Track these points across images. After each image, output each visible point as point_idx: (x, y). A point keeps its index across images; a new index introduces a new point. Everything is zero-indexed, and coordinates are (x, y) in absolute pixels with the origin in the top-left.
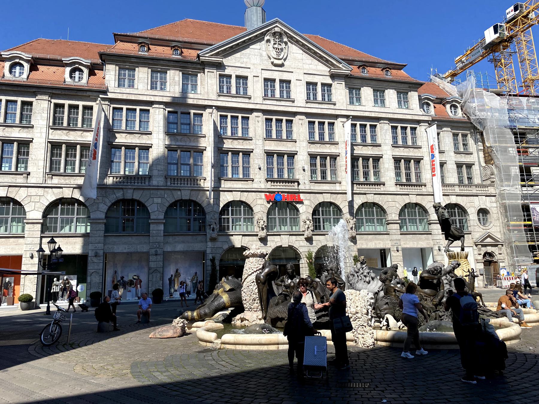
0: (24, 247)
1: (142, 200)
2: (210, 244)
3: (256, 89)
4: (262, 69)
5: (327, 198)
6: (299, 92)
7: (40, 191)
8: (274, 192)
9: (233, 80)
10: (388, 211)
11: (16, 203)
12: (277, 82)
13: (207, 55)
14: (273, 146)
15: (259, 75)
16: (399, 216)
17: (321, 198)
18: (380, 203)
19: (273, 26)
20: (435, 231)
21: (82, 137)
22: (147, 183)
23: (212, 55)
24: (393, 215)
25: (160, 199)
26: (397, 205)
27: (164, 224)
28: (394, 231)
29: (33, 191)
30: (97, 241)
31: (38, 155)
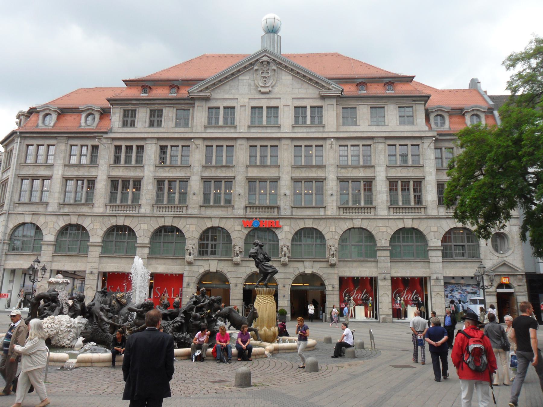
0: (89, 266)
1: (132, 226)
2: (187, 268)
3: (243, 118)
4: (249, 99)
5: (309, 224)
6: (286, 118)
7: (54, 218)
8: (252, 218)
9: (221, 111)
10: (377, 238)
11: (178, 230)
12: (265, 110)
13: (196, 92)
14: (254, 173)
15: (290, 103)
16: (442, 242)
17: (301, 225)
18: (368, 229)
19: (262, 56)
20: (434, 258)
21: (89, 172)
22: (184, 212)
23: (201, 91)
24: (383, 241)
25: (146, 225)
26: (389, 231)
27: (149, 248)
28: (383, 258)
29: (49, 218)
30: (93, 261)
31: (148, 189)
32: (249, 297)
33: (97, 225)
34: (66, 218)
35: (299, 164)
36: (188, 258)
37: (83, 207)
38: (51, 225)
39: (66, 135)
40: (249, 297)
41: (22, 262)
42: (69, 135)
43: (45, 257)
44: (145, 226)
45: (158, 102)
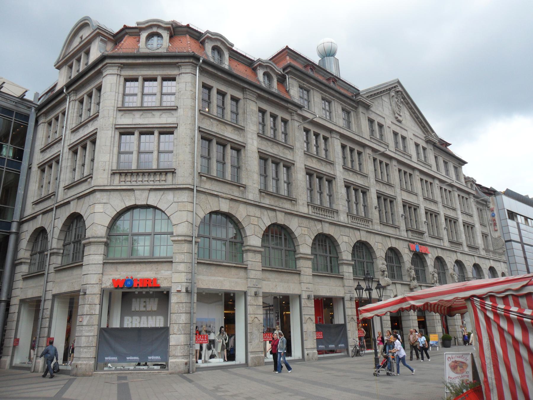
32: (201, 348)
33: (305, 231)
34: (272, 214)
35: (124, 167)
36: (406, 279)
37: (285, 201)
38: (254, 220)
39: (259, 92)
40: (201, 348)
41: (221, 279)
42: (262, 94)
43: (253, 272)
44: (346, 239)
45: (331, 91)
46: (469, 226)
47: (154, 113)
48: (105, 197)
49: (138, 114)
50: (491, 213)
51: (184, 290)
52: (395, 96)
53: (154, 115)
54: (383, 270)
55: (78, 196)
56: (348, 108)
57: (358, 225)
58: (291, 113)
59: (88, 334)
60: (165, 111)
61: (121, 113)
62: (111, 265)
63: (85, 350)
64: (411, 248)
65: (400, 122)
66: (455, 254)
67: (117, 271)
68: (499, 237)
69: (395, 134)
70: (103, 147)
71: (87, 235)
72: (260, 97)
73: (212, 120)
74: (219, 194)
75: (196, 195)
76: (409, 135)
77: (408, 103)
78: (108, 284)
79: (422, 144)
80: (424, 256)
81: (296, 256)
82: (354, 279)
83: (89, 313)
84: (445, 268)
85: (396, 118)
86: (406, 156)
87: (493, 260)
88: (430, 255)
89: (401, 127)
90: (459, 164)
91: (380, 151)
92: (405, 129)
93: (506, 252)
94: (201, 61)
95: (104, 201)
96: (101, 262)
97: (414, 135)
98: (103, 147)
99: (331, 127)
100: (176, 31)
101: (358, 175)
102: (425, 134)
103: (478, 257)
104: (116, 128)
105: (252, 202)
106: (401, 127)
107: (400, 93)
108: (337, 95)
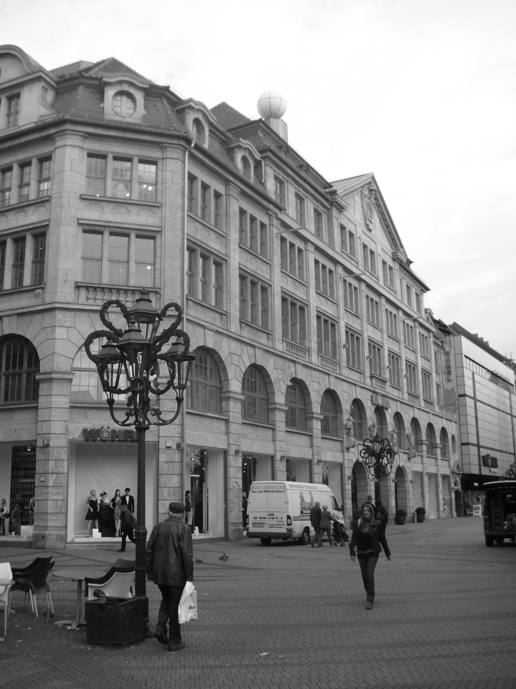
34: (251, 350)
46: (427, 374)
47: (130, 207)
48: (69, 319)
49: (108, 207)
50: (446, 357)
51: (174, 446)
52: (368, 196)
53: (129, 211)
54: (348, 427)
55: (19, 311)
56: (321, 209)
57: (327, 368)
58: (270, 215)
59: (56, 497)
60: (145, 207)
61: (86, 203)
62: (78, 410)
63: (53, 517)
64: (374, 399)
65: (370, 230)
66: (412, 409)
67: (87, 418)
68: (453, 389)
69: (365, 246)
70: (64, 249)
71: (42, 370)
72: (243, 193)
73: (196, 224)
74: (206, 324)
75: (187, 325)
76: (378, 250)
77: (379, 206)
78: (76, 434)
79: (390, 262)
80: (385, 410)
81: (270, 407)
82: (322, 437)
83: (55, 471)
84: (402, 428)
85: (367, 226)
86: (373, 278)
87: (446, 419)
88: (389, 410)
89: (370, 238)
90: (422, 290)
91: (355, 274)
92: (374, 242)
93: (457, 409)
94: (193, 145)
95: (68, 324)
96: (68, 406)
97: (382, 249)
98: (64, 249)
99: (308, 237)
100: (158, 94)
101: (328, 302)
102: (392, 248)
103: (433, 414)
104: (79, 224)
105: (235, 336)
106: (370, 238)
107: (374, 192)
108: (312, 191)
